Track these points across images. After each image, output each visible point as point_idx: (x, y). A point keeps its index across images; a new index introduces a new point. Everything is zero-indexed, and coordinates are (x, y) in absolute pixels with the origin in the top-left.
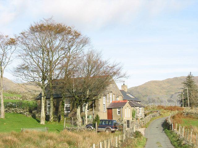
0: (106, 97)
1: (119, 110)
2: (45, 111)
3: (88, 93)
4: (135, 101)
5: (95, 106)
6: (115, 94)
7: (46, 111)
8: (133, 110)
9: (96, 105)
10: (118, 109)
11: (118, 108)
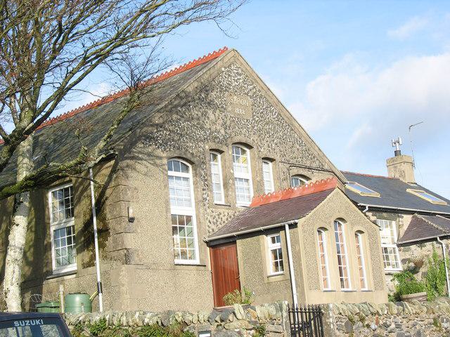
0: (195, 175)
1: (277, 246)
2: (262, 180)
3: (95, 228)
4: (420, 213)
5: (104, 232)
6: (277, 158)
7: (258, 179)
8: (435, 256)
9: (112, 224)
10: (267, 239)
11: (267, 232)
